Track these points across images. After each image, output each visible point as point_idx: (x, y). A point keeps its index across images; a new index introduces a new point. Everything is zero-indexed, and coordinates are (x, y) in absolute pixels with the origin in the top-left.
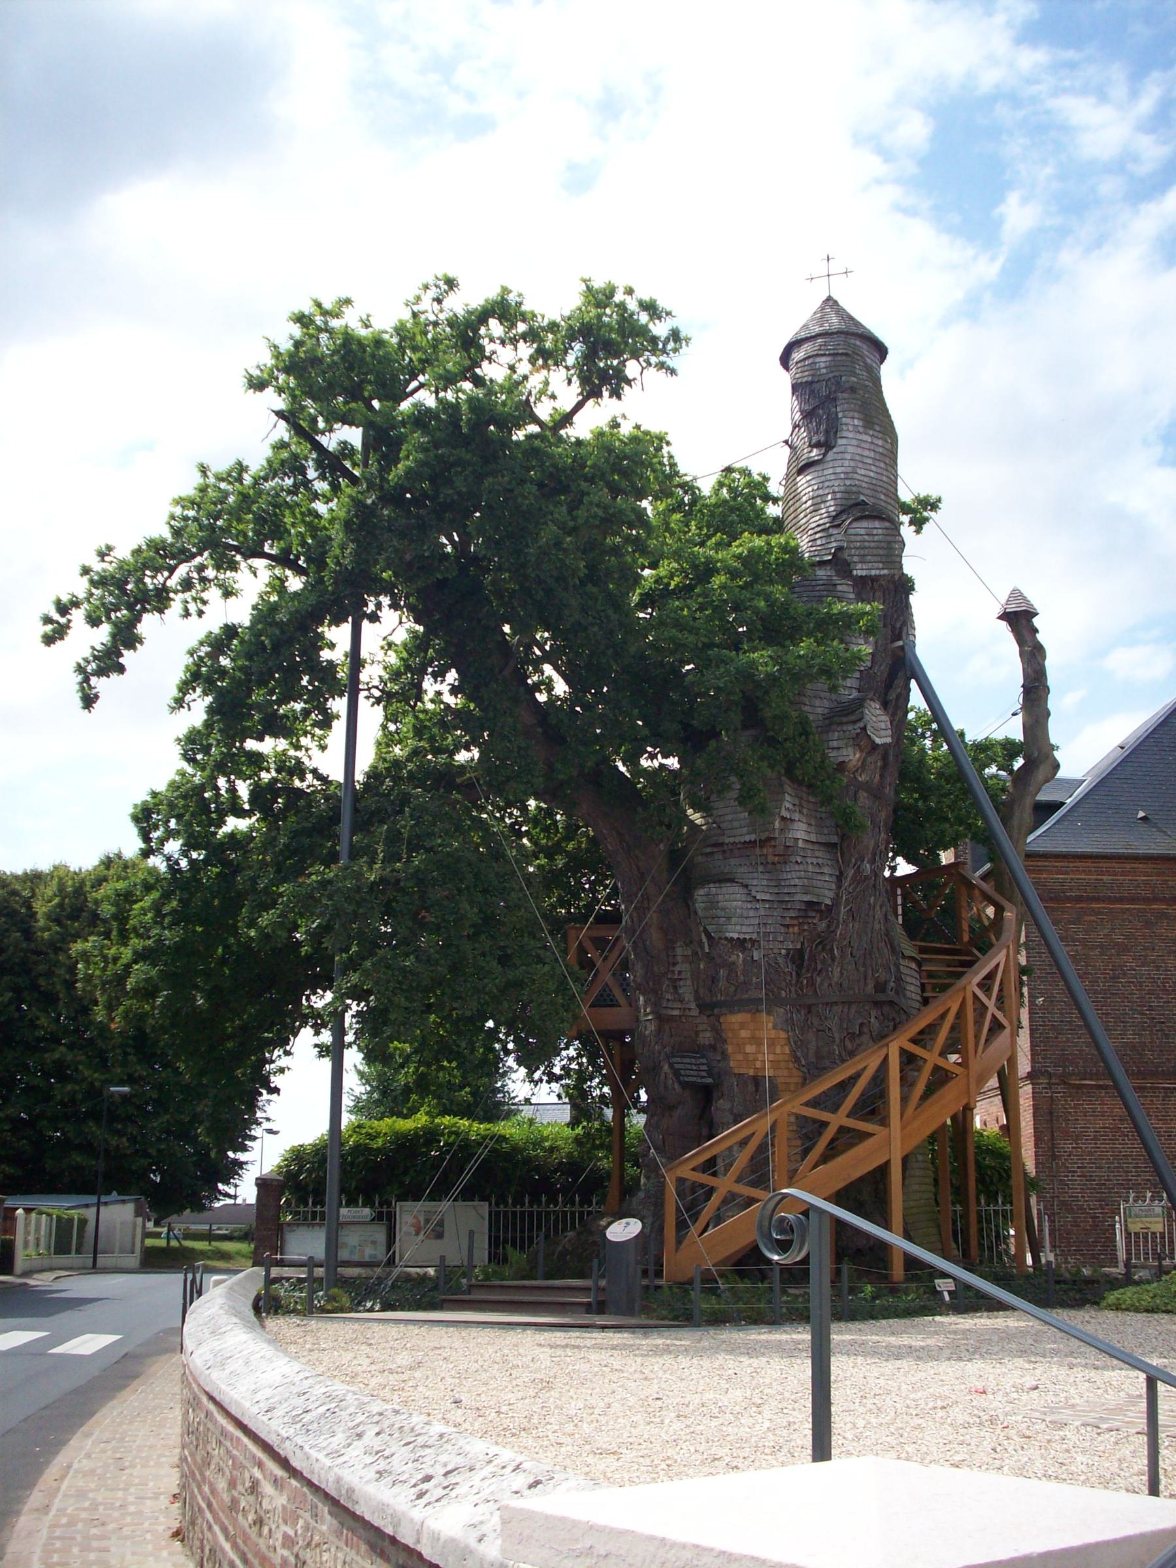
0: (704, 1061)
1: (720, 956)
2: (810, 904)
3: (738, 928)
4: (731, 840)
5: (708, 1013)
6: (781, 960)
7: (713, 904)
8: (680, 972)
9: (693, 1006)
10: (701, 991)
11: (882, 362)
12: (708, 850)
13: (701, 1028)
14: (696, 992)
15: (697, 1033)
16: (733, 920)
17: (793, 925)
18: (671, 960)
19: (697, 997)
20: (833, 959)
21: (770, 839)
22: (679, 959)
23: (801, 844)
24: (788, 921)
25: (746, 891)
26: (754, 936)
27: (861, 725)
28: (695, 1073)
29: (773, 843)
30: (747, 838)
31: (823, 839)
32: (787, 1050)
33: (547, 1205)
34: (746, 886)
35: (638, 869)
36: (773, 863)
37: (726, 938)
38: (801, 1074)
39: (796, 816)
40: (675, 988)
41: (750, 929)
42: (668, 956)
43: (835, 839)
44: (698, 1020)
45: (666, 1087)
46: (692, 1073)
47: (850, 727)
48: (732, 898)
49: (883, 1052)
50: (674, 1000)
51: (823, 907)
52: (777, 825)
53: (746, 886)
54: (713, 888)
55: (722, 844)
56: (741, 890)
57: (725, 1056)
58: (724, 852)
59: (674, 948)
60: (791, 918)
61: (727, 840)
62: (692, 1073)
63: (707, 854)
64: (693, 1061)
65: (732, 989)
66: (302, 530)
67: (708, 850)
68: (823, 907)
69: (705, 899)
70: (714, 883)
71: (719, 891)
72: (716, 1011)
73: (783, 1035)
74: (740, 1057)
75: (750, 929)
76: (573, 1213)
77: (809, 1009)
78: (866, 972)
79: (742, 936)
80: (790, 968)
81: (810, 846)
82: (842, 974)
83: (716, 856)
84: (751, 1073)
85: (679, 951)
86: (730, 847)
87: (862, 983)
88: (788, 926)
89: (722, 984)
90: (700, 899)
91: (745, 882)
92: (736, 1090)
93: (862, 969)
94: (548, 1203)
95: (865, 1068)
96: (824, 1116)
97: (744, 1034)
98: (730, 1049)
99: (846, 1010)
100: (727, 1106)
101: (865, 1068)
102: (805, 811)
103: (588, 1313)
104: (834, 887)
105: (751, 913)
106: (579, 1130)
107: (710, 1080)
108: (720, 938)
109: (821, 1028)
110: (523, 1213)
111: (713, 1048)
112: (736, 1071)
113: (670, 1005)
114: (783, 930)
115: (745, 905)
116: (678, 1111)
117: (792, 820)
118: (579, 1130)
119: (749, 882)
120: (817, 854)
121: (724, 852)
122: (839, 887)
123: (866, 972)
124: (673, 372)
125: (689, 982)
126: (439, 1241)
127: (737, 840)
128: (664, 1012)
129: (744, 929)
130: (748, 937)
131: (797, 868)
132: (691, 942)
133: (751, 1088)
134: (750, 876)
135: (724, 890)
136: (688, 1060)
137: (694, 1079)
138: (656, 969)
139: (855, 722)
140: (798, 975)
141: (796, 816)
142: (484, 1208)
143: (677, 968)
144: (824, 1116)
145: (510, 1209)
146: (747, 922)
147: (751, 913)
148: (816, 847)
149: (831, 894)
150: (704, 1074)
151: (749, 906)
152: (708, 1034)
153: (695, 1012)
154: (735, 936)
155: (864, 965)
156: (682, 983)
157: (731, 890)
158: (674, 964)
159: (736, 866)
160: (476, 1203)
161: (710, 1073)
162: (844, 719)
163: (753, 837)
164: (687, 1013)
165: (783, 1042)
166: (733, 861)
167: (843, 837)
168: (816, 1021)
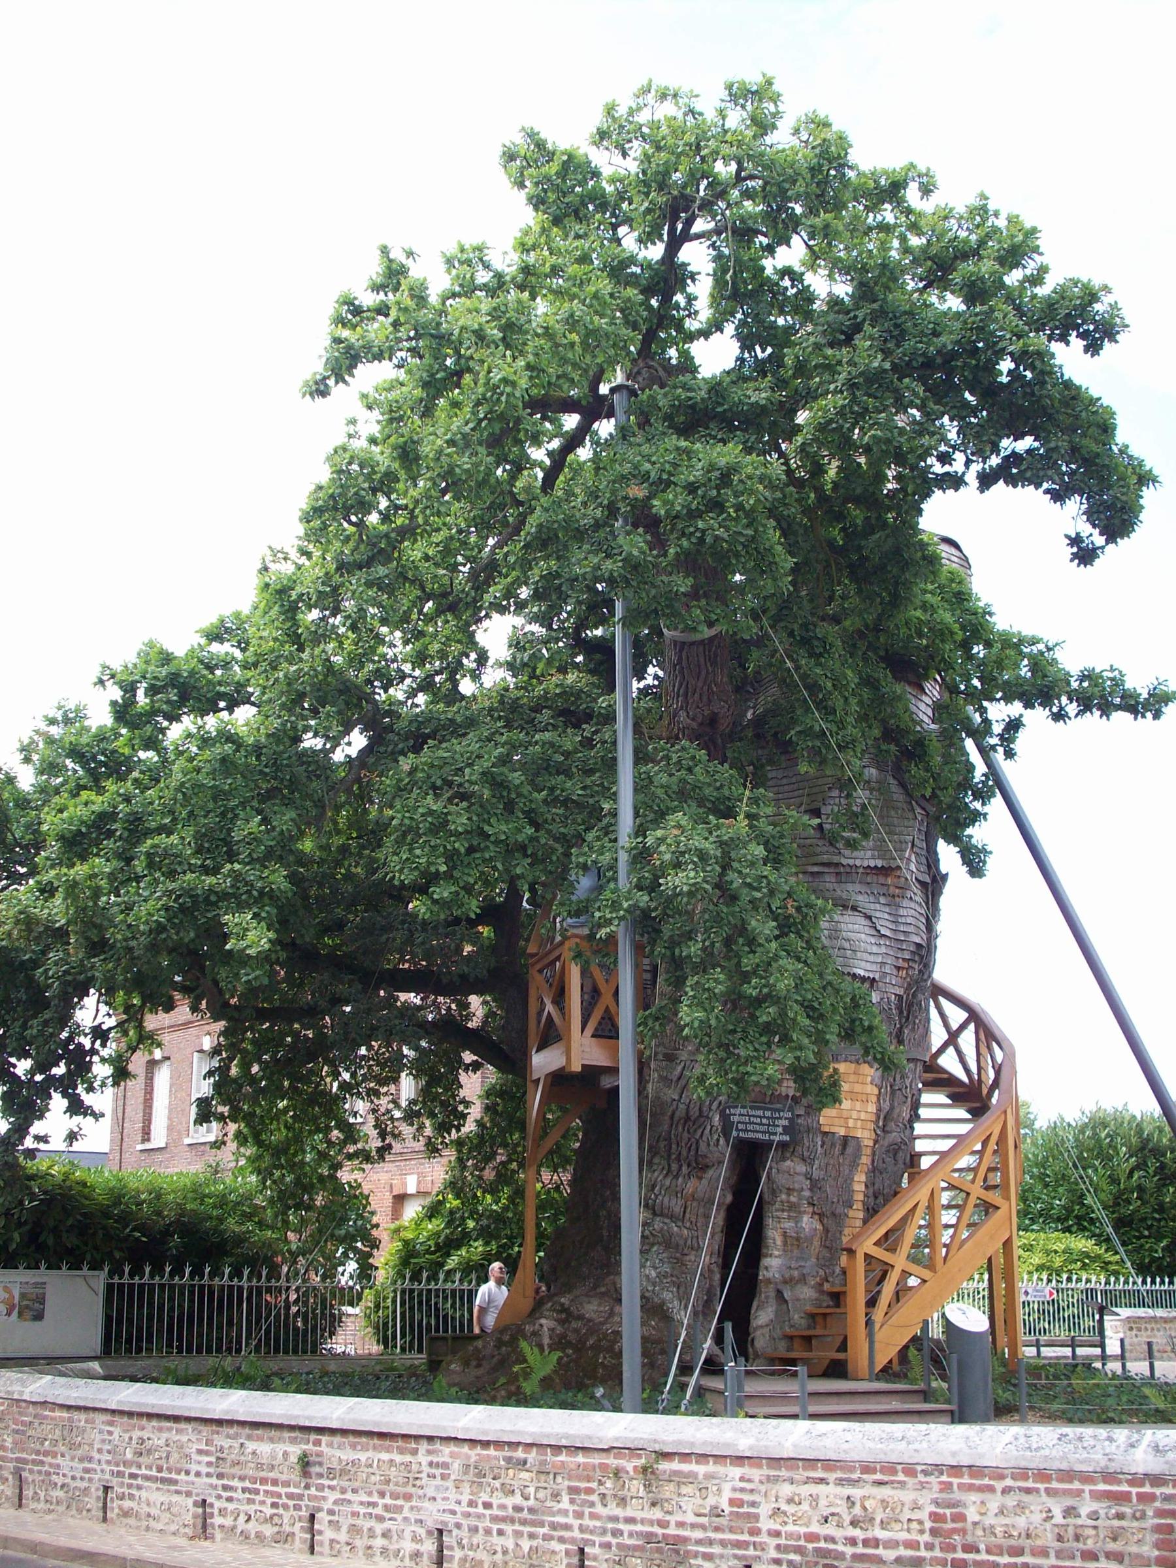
4: (851, 862)
7: (835, 934)
12: (816, 869)
24: (901, 963)
25: (867, 923)
30: (872, 863)
33: (211, 1278)
34: (869, 918)
41: (869, 967)
43: (928, 880)
46: (758, 1128)
48: (854, 928)
55: (837, 865)
56: (863, 921)
61: (844, 861)
62: (758, 1128)
63: (812, 873)
66: (653, 474)
67: (816, 869)
76: (403, 1292)
91: (869, 913)
94: (212, 1275)
100: (801, 1168)
103: (953, 1422)
105: (875, 949)
110: (141, 1286)
119: (873, 913)
126: (37, 1323)
135: (846, 918)
137: (759, 1136)
142: (99, 1279)
145: (126, 1280)
146: (871, 958)
147: (875, 949)
154: (862, 973)
157: (853, 919)
159: (855, 892)
160: (85, 1271)
163: (880, 863)
166: (850, 887)
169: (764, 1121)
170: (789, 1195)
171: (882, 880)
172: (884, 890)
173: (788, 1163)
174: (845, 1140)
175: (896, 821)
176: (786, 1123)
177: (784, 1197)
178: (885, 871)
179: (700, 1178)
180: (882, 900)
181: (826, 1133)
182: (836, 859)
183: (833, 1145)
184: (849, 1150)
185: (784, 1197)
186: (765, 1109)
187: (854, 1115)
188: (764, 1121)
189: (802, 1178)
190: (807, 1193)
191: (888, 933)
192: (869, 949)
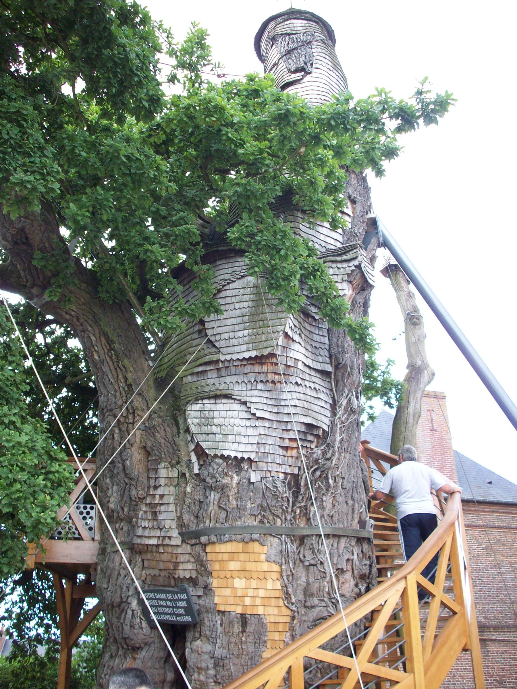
0: (184, 596)
1: (213, 477)
2: (310, 426)
3: (235, 446)
4: (228, 357)
5: (193, 542)
6: (279, 484)
8: (162, 496)
9: (175, 533)
10: (186, 517)
11: (334, 45)
12: (201, 369)
13: (181, 559)
14: (179, 518)
15: (176, 564)
16: (231, 438)
17: (292, 448)
18: (152, 483)
19: (181, 525)
20: (328, 487)
21: (272, 355)
22: (162, 482)
23: (300, 365)
24: (287, 443)
25: (244, 408)
26: (253, 456)
27: (356, 263)
28: (169, 610)
29: (274, 360)
30: (247, 355)
31: (319, 367)
32: (278, 585)
34: (245, 403)
35: (126, 379)
36: (273, 382)
37: (222, 456)
38: (289, 613)
39: (297, 338)
40: (155, 514)
41: (249, 448)
42: (149, 478)
43: (329, 368)
44: (179, 551)
45: (132, 626)
46: (167, 610)
47: (345, 265)
49: (401, 586)
50: (153, 528)
51: (321, 433)
52: (280, 342)
53: (245, 403)
54: (208, 404)
55: (217, 362)
56: (239, 407)
57: (207, 589)
58: (219, 370)
59: (156, 470)
60: (291, 439)
61: (222, 358)
62: (167, 610)
63: (198, 373)
64: (169, 596)
65: (223, 515)
67: (201, 369)
68: (321, 433)
69: (198, 414)
70: (209, 398)
71: (213, 407)
72: (204, 539)
73: (276, 568)
74: (228, 592)
75: (249, 448)
77: (302, 540)
78: (353, 505)
79: (239, 456)
80: (288, 494)
81: (307, 370)
82: (334, 506)
83: (209, 375)
84: (239, 610)
85: (163, 473)
86: (226, 364)
87: (350, 517)
88: (286, 448)
89: (213, 508)
90: (192, 414)
91: (243, 399)
92: (220, 630)
93: (350, 502)
95: (382, 606)
96: (343, 661)
97: (233, 566)
98: (215, 583)
99: (335, 545)
100: (207, 647)
101: (382, 606)
102: (303, 335)
104: (328, 414)
105: (250, 431)
106: (16, 664)
107: (188, 619)
108: (216, 456)
109: (313, 562)
111: (194, 582)
112: (222, 608)
113: (146, 533)
114: (281, 452)
115: (243, 423)
116: (143, 653)
117: (293, 340)
118: (16, 664)
119: (249, 399)
120: (314, 379)
121: (219, 370)
122: (334, 413)
123: (353, 505)
124: (170, 28)
125: (172, 507)
127: (235, 357)
128: (139, 541)
129: (242, 448)
130: (246, 456)
131: (297, 389)
132: (178, 463)
133: (237, 628)
134: (249, 393)
135: (220, 407)
136: (163, 596)
138: (134, 492)
139: (349, 261)
140: (294, 504)
141: (297, 338)
143: (159, 492)
144: (343, 661)
146: (246, 440)
147: (250, 431)
148: (313, 373)
149: (327, 421)
150: (182, 611)
151: (248, 423)
152: (190, 566)
153: (178, 541)
154: (233, 454)
155: (352, 498)
156: (162, 508)
157: (227, 407)
158: (156, 488)
161: (189, 610)
162: (339, 259)
163: (253, 354)
164: (167, 541)
165: (275, 576)
166: (228, 379)
167: (337, 367)
168: (309, 556)
169: (169, 604)
170: (199, 673)
171: (258, 368)
172: (262, 377)
173: (199, 642)
174: (244, 619)
175: (269, 316)
176: (184, 604)
177: (196, 675)
178: (259, 360)
179: (135, 659)
180: (260, 386)
181: (223, 612)
182: (215, 357)
183: (231, 623)
184: (250, 629)
185: (196, 675)
186: (166, 592)
187: (251, 593)
188: (169, 604)
189: (206, 657)
190: (212, 672)
191: (267, 415)
192: (243, 431)
